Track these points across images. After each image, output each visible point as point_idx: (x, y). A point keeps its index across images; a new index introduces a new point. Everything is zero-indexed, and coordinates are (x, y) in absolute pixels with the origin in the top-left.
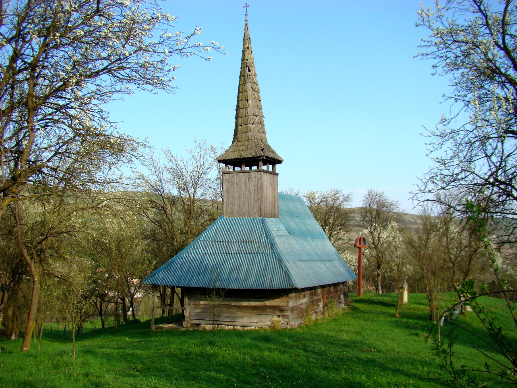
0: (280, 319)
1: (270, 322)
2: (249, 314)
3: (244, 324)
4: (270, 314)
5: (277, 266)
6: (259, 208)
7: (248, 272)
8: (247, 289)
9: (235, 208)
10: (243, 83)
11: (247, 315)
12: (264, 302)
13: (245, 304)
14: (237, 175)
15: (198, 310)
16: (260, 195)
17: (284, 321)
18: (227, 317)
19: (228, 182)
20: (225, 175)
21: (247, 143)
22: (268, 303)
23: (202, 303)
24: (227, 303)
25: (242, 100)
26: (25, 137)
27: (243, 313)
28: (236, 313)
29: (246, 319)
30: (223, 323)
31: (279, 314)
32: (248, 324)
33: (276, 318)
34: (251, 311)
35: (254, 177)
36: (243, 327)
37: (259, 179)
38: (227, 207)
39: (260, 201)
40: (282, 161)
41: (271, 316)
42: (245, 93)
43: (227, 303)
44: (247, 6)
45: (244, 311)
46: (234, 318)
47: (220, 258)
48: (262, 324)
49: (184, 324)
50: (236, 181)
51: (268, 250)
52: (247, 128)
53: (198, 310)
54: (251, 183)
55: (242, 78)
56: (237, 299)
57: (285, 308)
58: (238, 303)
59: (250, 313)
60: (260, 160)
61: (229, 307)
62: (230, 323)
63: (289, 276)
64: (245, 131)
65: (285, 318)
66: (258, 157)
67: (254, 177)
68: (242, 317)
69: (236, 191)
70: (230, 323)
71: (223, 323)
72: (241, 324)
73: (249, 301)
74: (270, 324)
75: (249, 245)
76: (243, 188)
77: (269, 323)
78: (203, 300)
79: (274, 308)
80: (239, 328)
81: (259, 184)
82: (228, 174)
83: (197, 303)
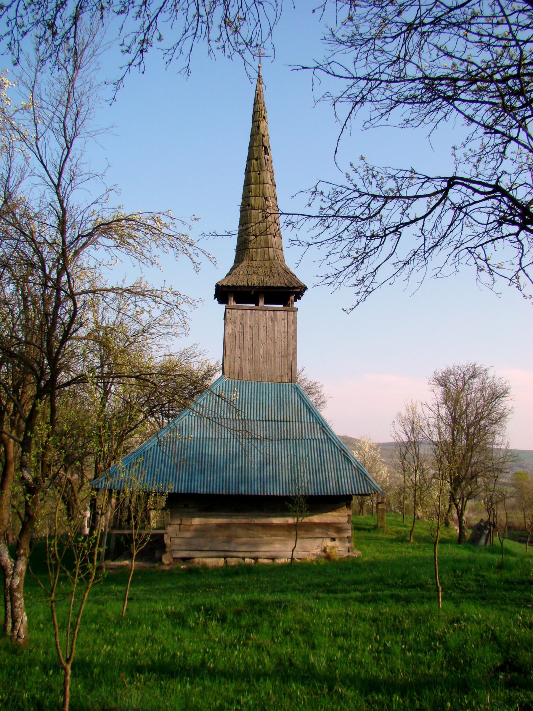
0: (337, 543)
1: (319, 550)
2: (283, 538)
3: (273, 554)
4: (320, 535)
5: (341, 459)
6: (289, 368)
7: (293, 469)
8: (191, 494)
9: (247, 367)
10: (256, 169)
11: (278, 540)
12: (310, 518)
13: (277, 521)
14: (251, 313)
15: (188, 535)
16: (290, 348)
17: (343, 547)
18: (243, 544)
19: (235, 323)
20: (230, 311)
21: (268, 264)
22: (316, 519)
23: (197, 521)
24: (244, 521)
25: (255, 196)
26: (376, 74)
27: (272, 536)
28: (259, 537)
29: (277, 547)
30: (235, 554)
31: (334, 535)
32: (281, 554)
33: (329, 543)
34: (287, 533)
35: (282, 319)
36: (273, 559)
37: (290, 323)
38: (232, 364)
39: (291, 357)
40: (305, 288)
41: (321, 540)
42: (261, 186)
43: (244, 521)
44: (351, 165)
45: (273, 532)
46: (255, 544)
47: (234, 447)
48: (306, 553)
49: (166, 559)
50: (248, 321)
51: (319, 435)
52: (267, 241)
53: (188, 535)
54: (276, 328)
55: (254, 161)
56: (262, 514)
57: (345, 525)
58: (264, 521)
59: (284, 535)
60: (293, 293)
61: (248, 527)
62: (248, 554)
63: (365, 475)
64: (263, 245)
65: (344, 542)
66: (288, 287)
67: (282, 319)
68: (271, 543)
69: (249, 339)
70: (248, 554)
71: (235, 554)
72: (268, 554)
73: (283, 516)
74: (319, 553)
75: (284, 426)
76: (262, 335)
77: (318, 551)
78: (199, 516)
79: (326, 526)
80: (266, 561)
81: (290, 330)
82: (235, 311)
83: (186, 522)
